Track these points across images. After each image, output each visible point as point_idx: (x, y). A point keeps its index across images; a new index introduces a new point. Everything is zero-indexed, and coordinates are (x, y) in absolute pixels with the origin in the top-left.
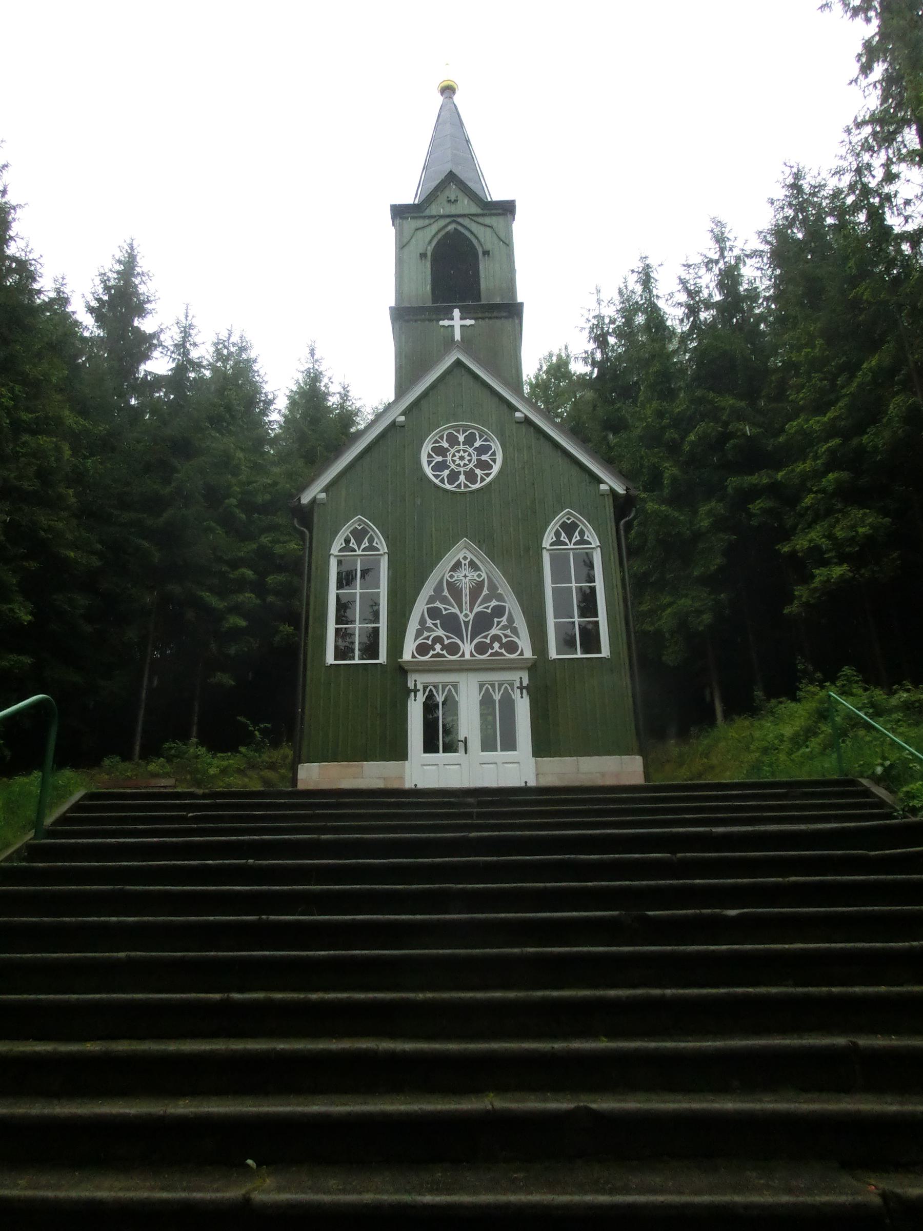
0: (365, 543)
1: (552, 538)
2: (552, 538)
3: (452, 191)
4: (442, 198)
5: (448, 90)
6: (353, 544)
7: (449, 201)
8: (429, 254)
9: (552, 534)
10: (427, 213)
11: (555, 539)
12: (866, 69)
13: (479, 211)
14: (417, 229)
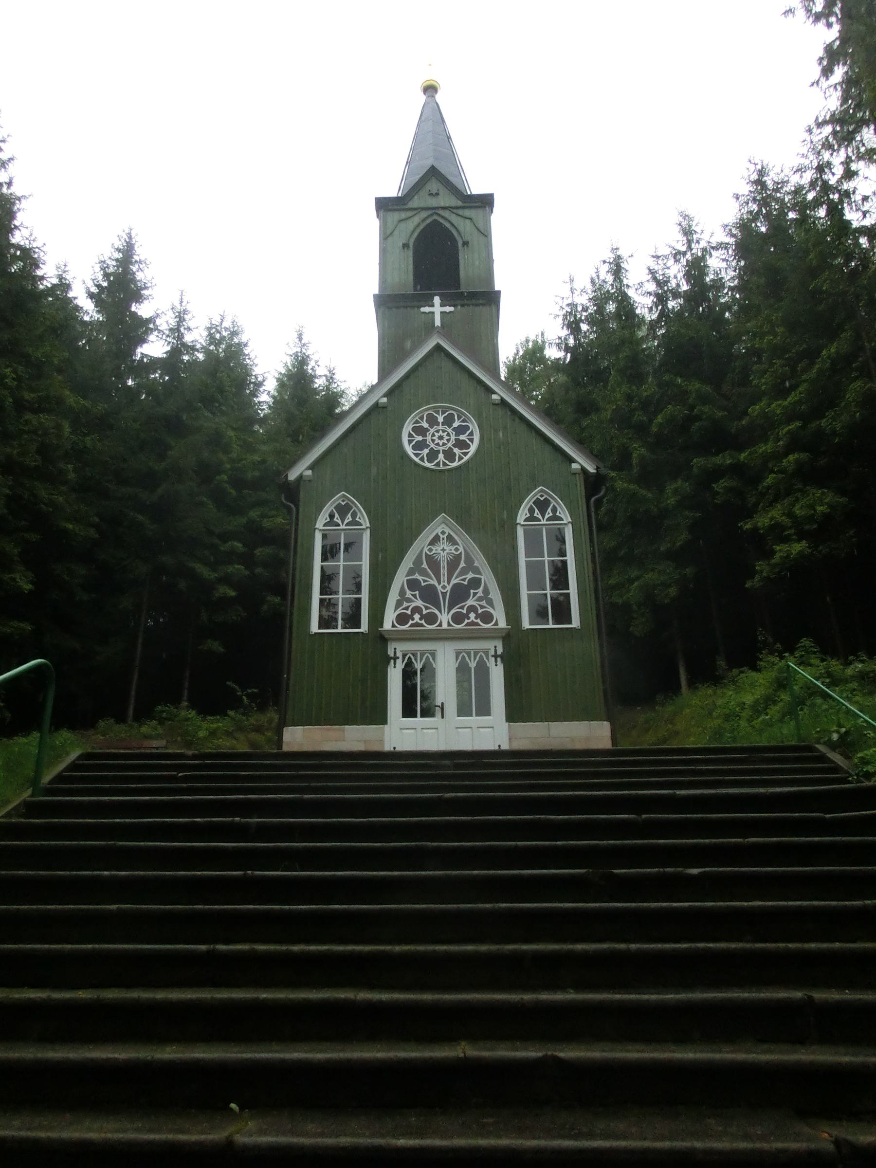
0: (349, 518)
1: (326, 519)
2: (326, 519)
4: (424, 193)
6: (337, 519)
7: (431, 194)
8: (411, 245)
11: (528, 515)
12: (827, 72)
13: (460, 203)
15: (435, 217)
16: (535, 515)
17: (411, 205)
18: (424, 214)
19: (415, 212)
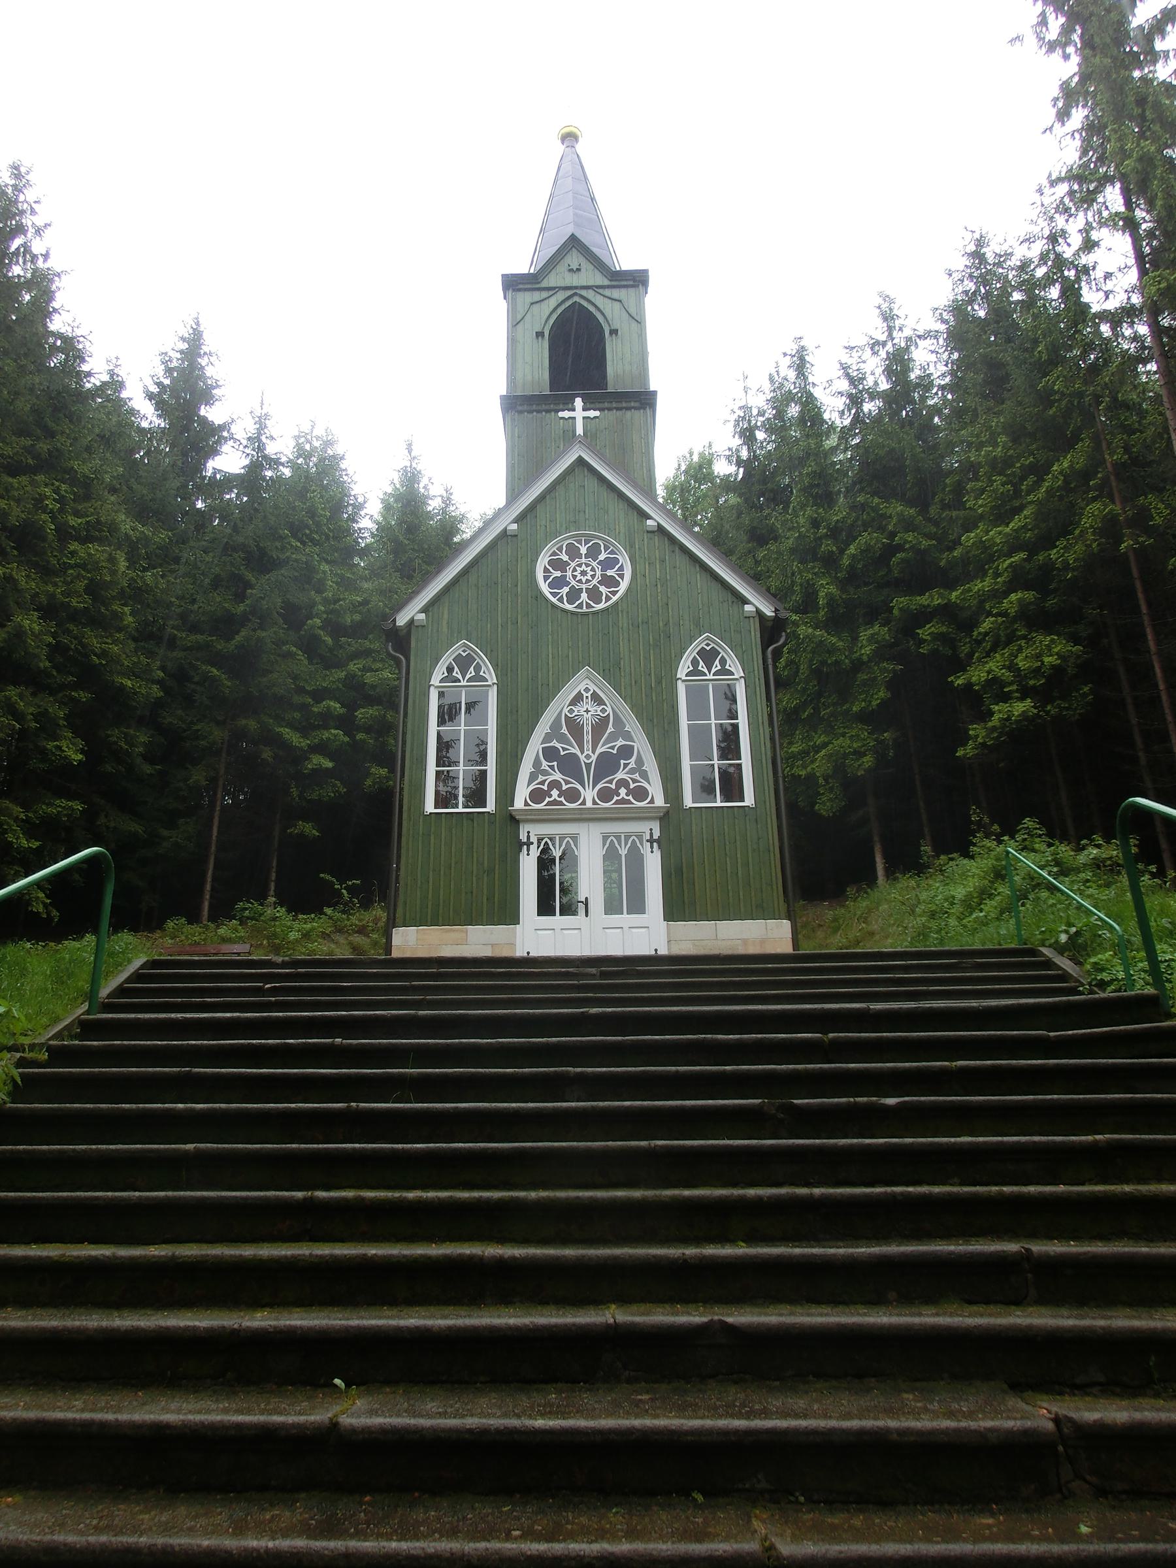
0: (471, 672)
3: (574, 259)
4: (562, 268)
5: (569, 138)
7: (571, 270)
9: (689, 663)
10: (544, 284)
13: (606, 282)
14: (532, 304)
15: (576, 299)
16: (700, 668)
17: (552, 280)
18: (561, 296)
19: (551, 293)
